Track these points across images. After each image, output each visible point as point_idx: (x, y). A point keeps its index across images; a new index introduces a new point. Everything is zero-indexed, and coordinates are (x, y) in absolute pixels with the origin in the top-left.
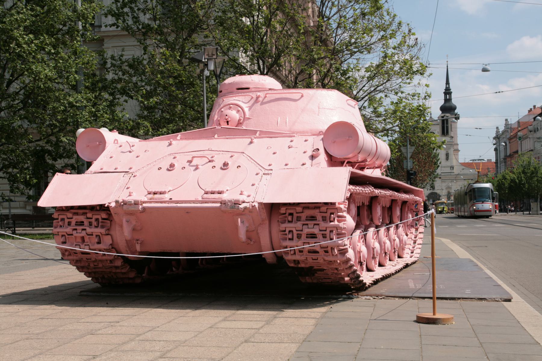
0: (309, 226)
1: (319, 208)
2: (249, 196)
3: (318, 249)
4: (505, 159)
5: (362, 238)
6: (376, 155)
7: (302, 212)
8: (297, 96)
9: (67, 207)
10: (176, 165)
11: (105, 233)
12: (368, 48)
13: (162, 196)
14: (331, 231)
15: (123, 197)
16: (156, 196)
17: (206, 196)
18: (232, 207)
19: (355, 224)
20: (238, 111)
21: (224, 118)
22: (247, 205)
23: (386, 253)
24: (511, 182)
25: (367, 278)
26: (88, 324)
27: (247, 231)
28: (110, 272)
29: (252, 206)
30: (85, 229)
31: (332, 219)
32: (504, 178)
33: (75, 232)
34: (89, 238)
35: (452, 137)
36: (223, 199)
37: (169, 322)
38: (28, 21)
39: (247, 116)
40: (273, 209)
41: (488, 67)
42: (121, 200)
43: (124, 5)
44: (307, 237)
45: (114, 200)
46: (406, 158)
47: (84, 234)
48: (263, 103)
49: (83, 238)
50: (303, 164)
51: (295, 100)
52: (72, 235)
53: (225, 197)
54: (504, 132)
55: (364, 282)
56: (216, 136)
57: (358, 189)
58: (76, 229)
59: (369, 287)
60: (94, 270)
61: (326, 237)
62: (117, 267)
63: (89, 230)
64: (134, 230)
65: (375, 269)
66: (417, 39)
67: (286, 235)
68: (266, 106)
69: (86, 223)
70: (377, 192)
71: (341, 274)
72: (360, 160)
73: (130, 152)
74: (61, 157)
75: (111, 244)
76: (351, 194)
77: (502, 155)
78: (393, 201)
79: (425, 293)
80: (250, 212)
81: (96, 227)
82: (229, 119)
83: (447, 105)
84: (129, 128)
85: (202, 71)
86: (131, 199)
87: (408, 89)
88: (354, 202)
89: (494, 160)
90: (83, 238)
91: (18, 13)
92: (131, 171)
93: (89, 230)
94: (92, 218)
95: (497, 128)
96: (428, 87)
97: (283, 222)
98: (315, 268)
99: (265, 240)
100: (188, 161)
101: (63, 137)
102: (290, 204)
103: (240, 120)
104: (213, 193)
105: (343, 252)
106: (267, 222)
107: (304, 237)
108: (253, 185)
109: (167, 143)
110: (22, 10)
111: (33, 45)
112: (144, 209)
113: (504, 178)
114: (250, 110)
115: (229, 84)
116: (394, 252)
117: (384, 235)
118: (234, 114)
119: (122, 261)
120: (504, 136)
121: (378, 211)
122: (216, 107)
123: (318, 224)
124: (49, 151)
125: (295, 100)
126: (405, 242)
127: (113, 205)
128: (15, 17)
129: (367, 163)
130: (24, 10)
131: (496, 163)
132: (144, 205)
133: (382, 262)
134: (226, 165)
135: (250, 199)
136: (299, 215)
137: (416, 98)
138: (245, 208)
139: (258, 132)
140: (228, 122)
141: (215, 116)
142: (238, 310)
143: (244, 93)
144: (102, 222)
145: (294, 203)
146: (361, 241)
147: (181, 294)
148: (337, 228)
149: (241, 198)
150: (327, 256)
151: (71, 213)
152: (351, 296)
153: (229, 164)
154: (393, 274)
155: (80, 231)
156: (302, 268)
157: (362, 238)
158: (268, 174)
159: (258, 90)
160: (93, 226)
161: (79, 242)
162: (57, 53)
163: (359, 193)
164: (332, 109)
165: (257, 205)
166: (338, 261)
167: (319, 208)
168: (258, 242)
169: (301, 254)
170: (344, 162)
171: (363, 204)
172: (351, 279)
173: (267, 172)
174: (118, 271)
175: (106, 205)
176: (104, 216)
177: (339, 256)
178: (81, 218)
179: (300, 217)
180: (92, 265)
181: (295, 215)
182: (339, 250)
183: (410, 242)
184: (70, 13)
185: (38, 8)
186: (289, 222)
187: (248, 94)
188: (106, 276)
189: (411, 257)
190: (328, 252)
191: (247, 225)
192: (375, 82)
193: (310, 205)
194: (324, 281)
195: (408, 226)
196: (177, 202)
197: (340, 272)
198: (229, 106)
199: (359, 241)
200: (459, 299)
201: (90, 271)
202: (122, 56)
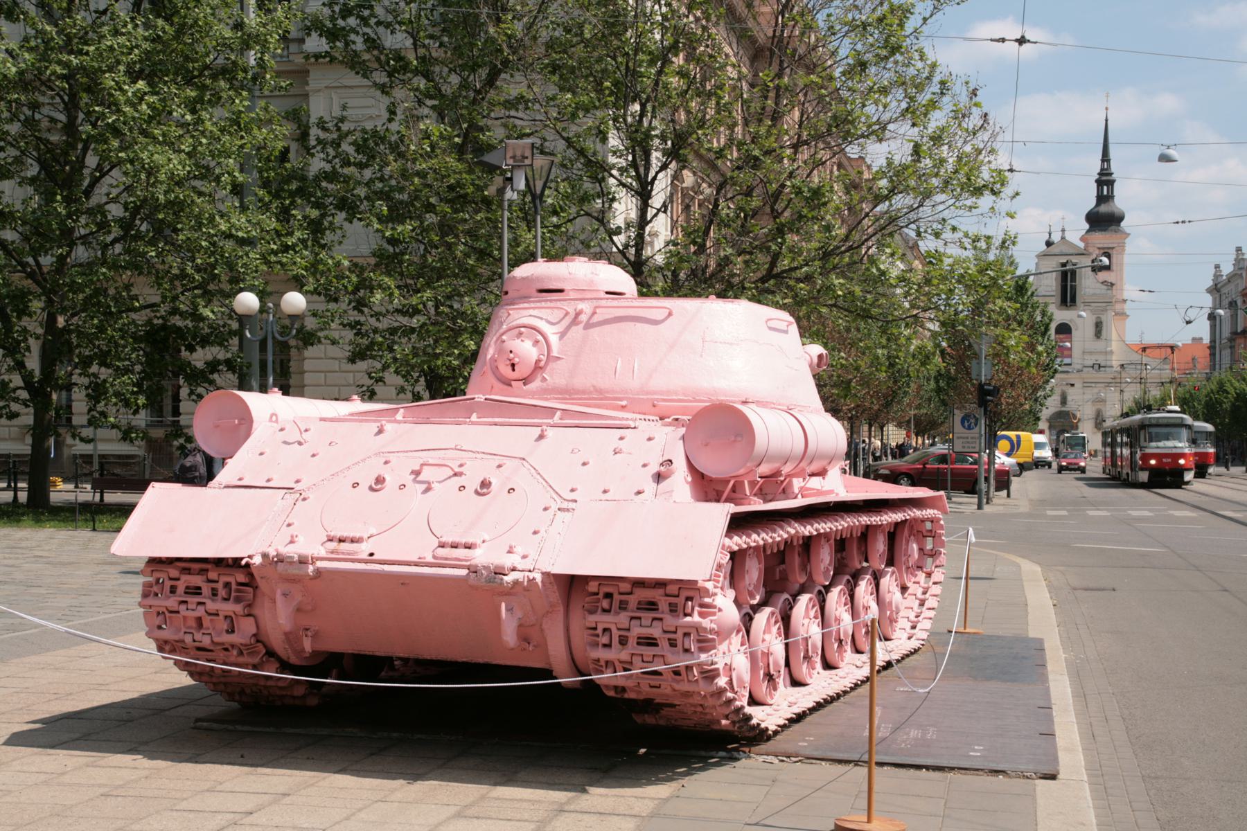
0: (644, 622)
2: (524, 557)
4: (1231, 340)
5: (776, 622)
7: (631, 593)
8: (658, 315)
10: (388, 478)
15: (278, 546)
16: (344, 546)
18: (489, 580)
20: (536, 342)
24: (1236, 399)
25: (767, 717)
26: (191, 816)
27: (520, 626)
28: (256, 685)
30: (204, 603)
31: (688, 610)
32: (1221, 388)
33: (183, 607)
35: (1112, 285)
36: (473, 562)
37: (347, 818)
38: (136, 51)
40: (572, 587)
41: (1171, 152)
43: (346, 12)
44: (638, 644)
46: (976, 356)
47: (200, 612)
48: (588, 326)
49: (199, 621)
50: (639, 493)
51: (656, 322)
52: (178, 612)
53: (480, 557)
54: (1231, 278)
56: (474, 418)
57: (757, 538)
58: (186, 602)
59: (776, 733)
60: (222, 680)
61: (675, 646)
63: (211, 606)
65: (808, 681)
66: (986, 115)
68: (594, 332)
69: (206, 590)
73: (300, 444)
74: (205, 342)
75: (254, 635)
77: (1226, 332)
79: (886, 754)
81: (226, 600)
83: (1104, 208)
84: (350, 288)
85: (501, 192)
86: (292, 551)
89: (1207, 340)
90: (199, 621)
91: (116, 33)
93: (211, 606)
95: (1217, 267)
96: (1012, 217)
97: (591, 612)
100: (413, 472)
101: (205, 307)
103: (538, 361)
104: (455, 546)
106: (561, 609)
107: (632, 642)
108: (535, 533)
110: (125, 26)
111: (144, 107)
112: (319, 573)
113: (1221, 388)
114: (561, 338)
115: (523, 279)
118: (527, 350)
120: (1231, 287)
122: (495, 327)
123: (661, 619)
124: (180, 328)
125: (656, 322)
126: (897, 608)
127: (257, 560)
128: (109, 43)
130: (130, 26)
131: (1212, 347)
132: (319, 564)
134: (485, 484)
135: (528, 564)
139: (558, 413)
140: (513, 365)
141: (490, 351)
142: (496, 784)
143: (551, 301)
144: (238, 591)
146: (775, 629)
147: (395, 735)
148: (698, 628)
149: (508, 561)
150: (678, 682)
151: (176, 568)
152: (735, 754)
154: (845, 692)
158: (568, 510)
159: (584, 293)
160: (219, 597)
161: (190, 627)
162: (200, 121)
165: (538, 577)
168: (542, 646)
172: (733, 723)
173: (565, 505)
177: (701, 683)
178: (196, 580)
179: (626, 603)
181: (617, 597)
184: (228, 33)
185: (160, 22)
186: (604, 611)
187: (558, 304)
188: (248, 691)
191: (519, 614)
195: (908, 568)
200: (952, 769)
201: (214, 680)
202: (342, 119)
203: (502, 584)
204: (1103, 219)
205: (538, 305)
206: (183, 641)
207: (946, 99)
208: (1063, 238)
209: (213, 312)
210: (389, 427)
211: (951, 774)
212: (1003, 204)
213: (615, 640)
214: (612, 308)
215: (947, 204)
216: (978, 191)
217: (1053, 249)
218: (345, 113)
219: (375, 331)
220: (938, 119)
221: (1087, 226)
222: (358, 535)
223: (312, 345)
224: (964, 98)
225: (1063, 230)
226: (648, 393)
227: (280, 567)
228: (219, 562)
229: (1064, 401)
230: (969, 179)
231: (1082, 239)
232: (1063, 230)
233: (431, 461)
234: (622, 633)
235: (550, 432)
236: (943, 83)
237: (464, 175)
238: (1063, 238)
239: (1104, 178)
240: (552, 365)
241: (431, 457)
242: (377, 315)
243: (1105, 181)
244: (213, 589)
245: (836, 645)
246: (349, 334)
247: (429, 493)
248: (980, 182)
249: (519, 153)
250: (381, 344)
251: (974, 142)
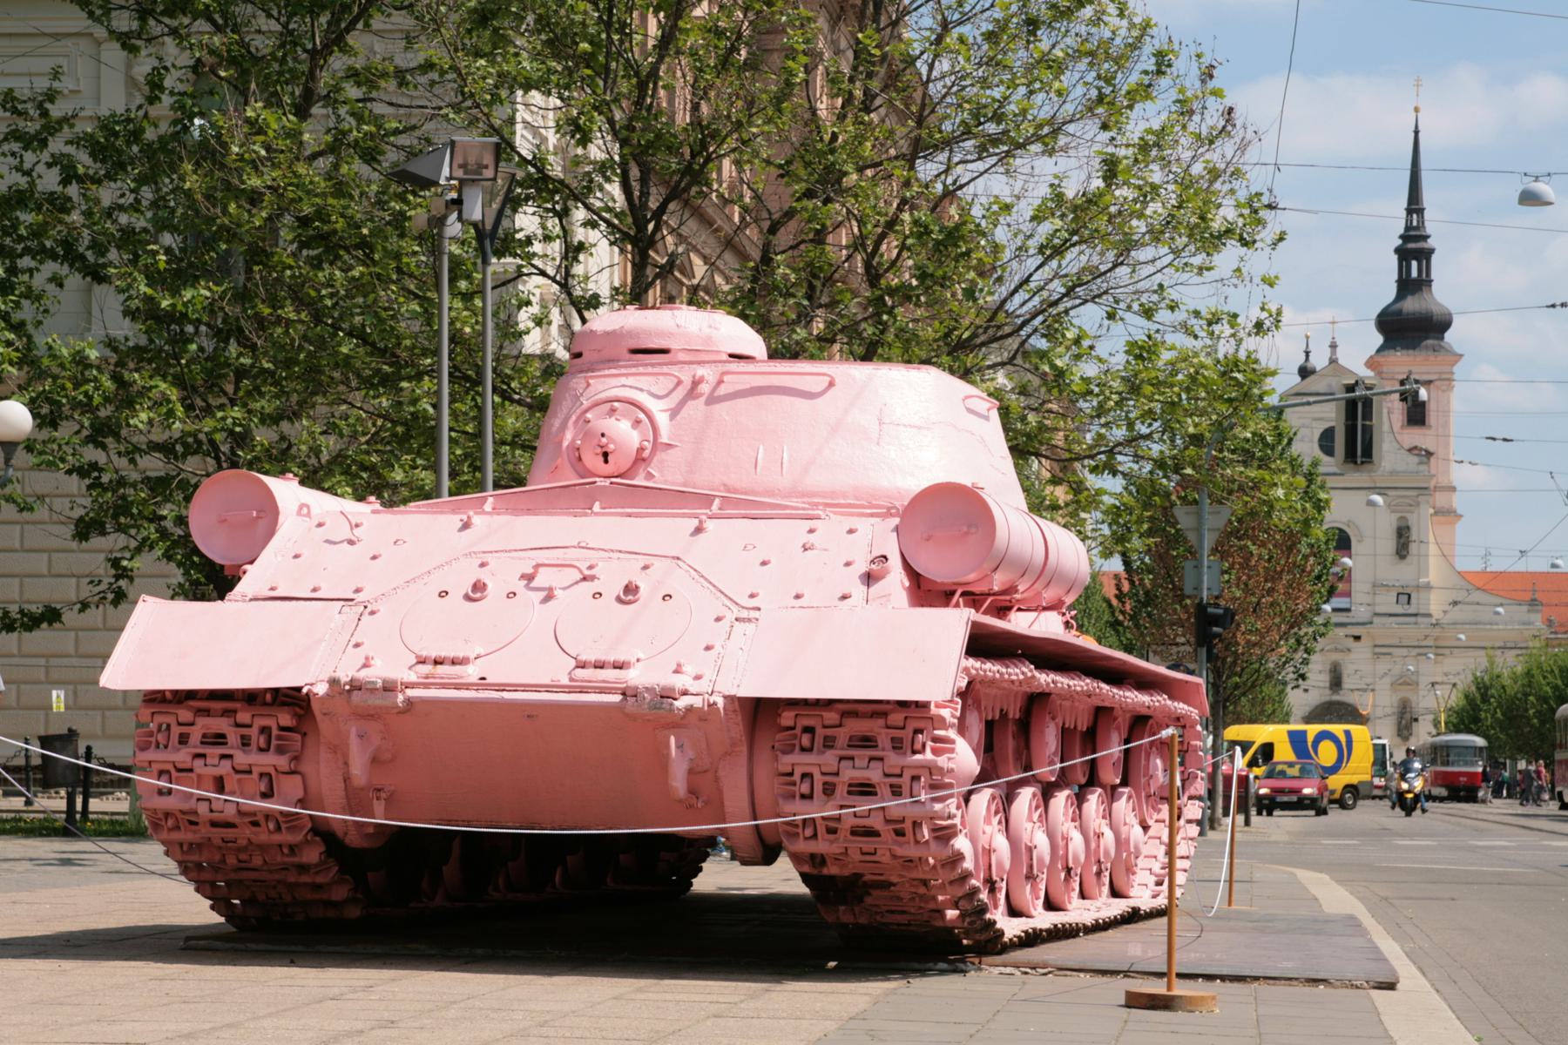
1: (885, 714)
2: (698, 678)
3: (876, 822)
5: (996, 813)
6: (1044, 572)
8: (816, 384)
9: (175, 693)
10: (490, 586)
11: (286, 769)
12: (1049, 136)
13: (457, 669)
14: (915, 778)
16: (441, 669)
17: (580, 673)
19: (977, 770)
20: (637, 422)
21: (596, 442)
22: (697, 702)
23: (1068, 870)
27: (691, 772)
29: (710, 705)
30: (230, 757)
31: (918, 746)
33: (198, 763)
34: (239, 781)
35: (1429, 454)
39: (664, 439)
40: (760, 713)
41: (1542, 188)
42: (344, 679)
44: (849, 793)
45: (326, 677)
46: (1193, 553)
47: (225, 768)
48: (712, 400)
50: (844, 597)
52: (191, 770)
53: (635, 677)
55: (998, 926)
56: (597, 507)
57: (991, 668)
58: (203, 756)
62: (303, 868)
63: (242, 759)
64: (375, 761)
66: (1231, 110)
67: (794, 784)
70: (1045, 679)
71: (934, 898)
72: (996, 588)
73: (351, 542)
76: (969, 683)
78: (1102, 713)
80: (700, 720)
82: (612, 446)
83: (1411, 305)
86: (377, 673)
87: (1195, 294)
88: (978, 704)
92: (360, 597)
93: (242, 759)
94: (250, 726)
96: (1271, 285)
97: (789, 750)
98: (868, 878)
99: (735, 793)
100: (523, 577)
102: (805, 703)
103: (641, 449)
104: (600, 666)
105: (945, 835)
106: (744, 749)
107: (841, 790)
108: (708, 648)
109: (456, 520)
112: (410, 702)
115: (607, 334)
116: (1099, 874)
117: (1065, 814)
118: (624, 433)
119: (323, 849)
121: (1049, 739)
123: (881, 759)
126: (1137, 848)
127: (321, 689)
129: (1018, 596)
132: (410, 693)
133: (1056, 895)
134: (631, 589)
136: (829, 732)
137: (1224, 329)
138: (690, 709)
139: (717, 502)
140: (606, 455)
143: (653, 365)
144: (279, 738)
145: (818, 701)
146: (995, 820)
147: (480, 951)
148: (931, 769)
149: (680, 682)
150: (901, 845)
151: (190, 708)
153: (642, 590)
155: (216, 761)
156: (832, 878)
157: (996, 813)
158: (749, 620)
159: (698, 356)
163: (993, 682)
164: (919, 428)
166: (931, 861)
167: (885, 714)
169: (832, 837)
170: (953, 593)
171: (1004, 715)
172: (962, 916)
173: (744, 614)
174: (305, 879)
175: (305, 690)
176: (286, 719)
177: (933, 845)
179: (834, 739)
180: (231, 860)
181: (820, 732)
182: (935, 830)
183: (1142, 842)
186: (803, 749)
187: (665, 369)
189: (1154, 897)
190: (903, 835)
191: (691, 754)
192: (1074, 260)
193: (861, 708)
194: (889, 918)
195: (1148, 796)
196: (502, 687)
197: (933, 892)
198: (611, 406)
199: (988, 821)
200: (1256, 978)
202: (51, 96)
203: (671, 710)
204: (1410, 326)
205: (633, 370)
206: (195, 813)
207: (1164, 82)
208: (1333, 361)
211: (1256, 984)
212: (1258, 261)
213: (818, 787)
214: (740, 378)
215: (1159, 264)
216: (1213, 241)
217: (1313, 384)
218: (56, 84)
220: (1144, 119)
221: (1379, 339)
222: (461, 655)
224: (1192, 83)
225: (1333, 346)
226: (803, 495)
227: (356, 696)
228: (251, 697)
229: (1336, 683)
230: (1203, 218)
231: (1370, 364)
232: (1333, 346)
234: (828, 778)
235: (710, 525)
236: (1160, 55)
237: (331, 201)
238: (1333, 361)
239: (1411, 246)
240: (660, 456)
243: (1414, 251)
244: (243, 737)
245: (1063, 875)
248: (1217, 225)
249: (472, 160)
251: (1208, 156)
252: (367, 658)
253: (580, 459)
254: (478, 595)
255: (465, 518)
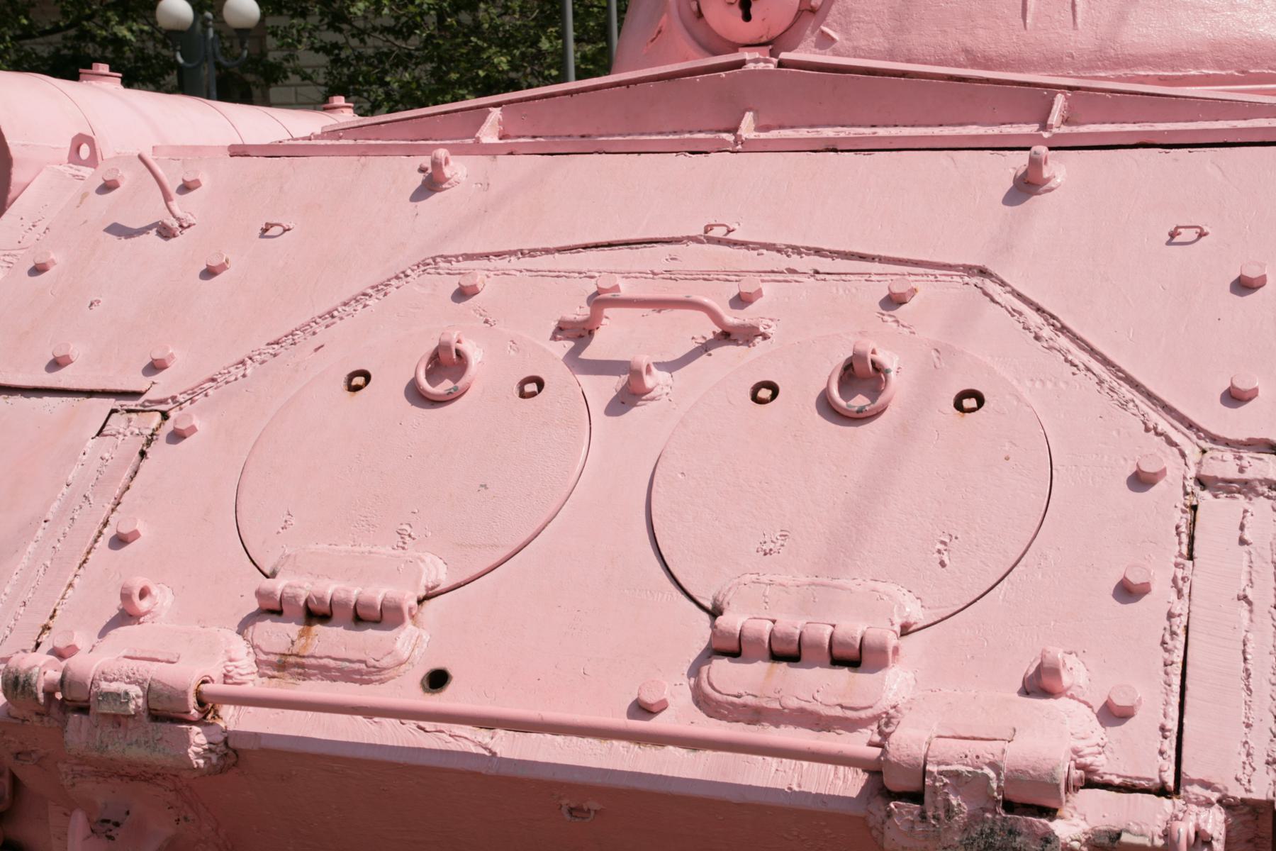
56: (747, 128)
73: (165, 232)
86: (108, 662)
100: (562, 330)
104: (787, 653)
109: (409, 171)
112: (233, 754)
132: (232, 719)
134: (861, 375)
173: (1224, 465)
209: (131, 30)
210: (458, 169)
219: (359, 57)
223: (276, 81)
226: (1118, 63)
227: (78, 732)
233: (627, 289)
235: (1059, 168)
241: (626, 273)
242: (360, 34)
246: (323, 59)
247: (638, 413)
250: (366, 75)
252: (126, 596)
253: (700, 14)
254: (444, 387)
255: (426, 161)
